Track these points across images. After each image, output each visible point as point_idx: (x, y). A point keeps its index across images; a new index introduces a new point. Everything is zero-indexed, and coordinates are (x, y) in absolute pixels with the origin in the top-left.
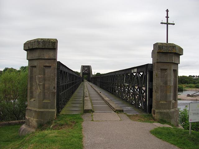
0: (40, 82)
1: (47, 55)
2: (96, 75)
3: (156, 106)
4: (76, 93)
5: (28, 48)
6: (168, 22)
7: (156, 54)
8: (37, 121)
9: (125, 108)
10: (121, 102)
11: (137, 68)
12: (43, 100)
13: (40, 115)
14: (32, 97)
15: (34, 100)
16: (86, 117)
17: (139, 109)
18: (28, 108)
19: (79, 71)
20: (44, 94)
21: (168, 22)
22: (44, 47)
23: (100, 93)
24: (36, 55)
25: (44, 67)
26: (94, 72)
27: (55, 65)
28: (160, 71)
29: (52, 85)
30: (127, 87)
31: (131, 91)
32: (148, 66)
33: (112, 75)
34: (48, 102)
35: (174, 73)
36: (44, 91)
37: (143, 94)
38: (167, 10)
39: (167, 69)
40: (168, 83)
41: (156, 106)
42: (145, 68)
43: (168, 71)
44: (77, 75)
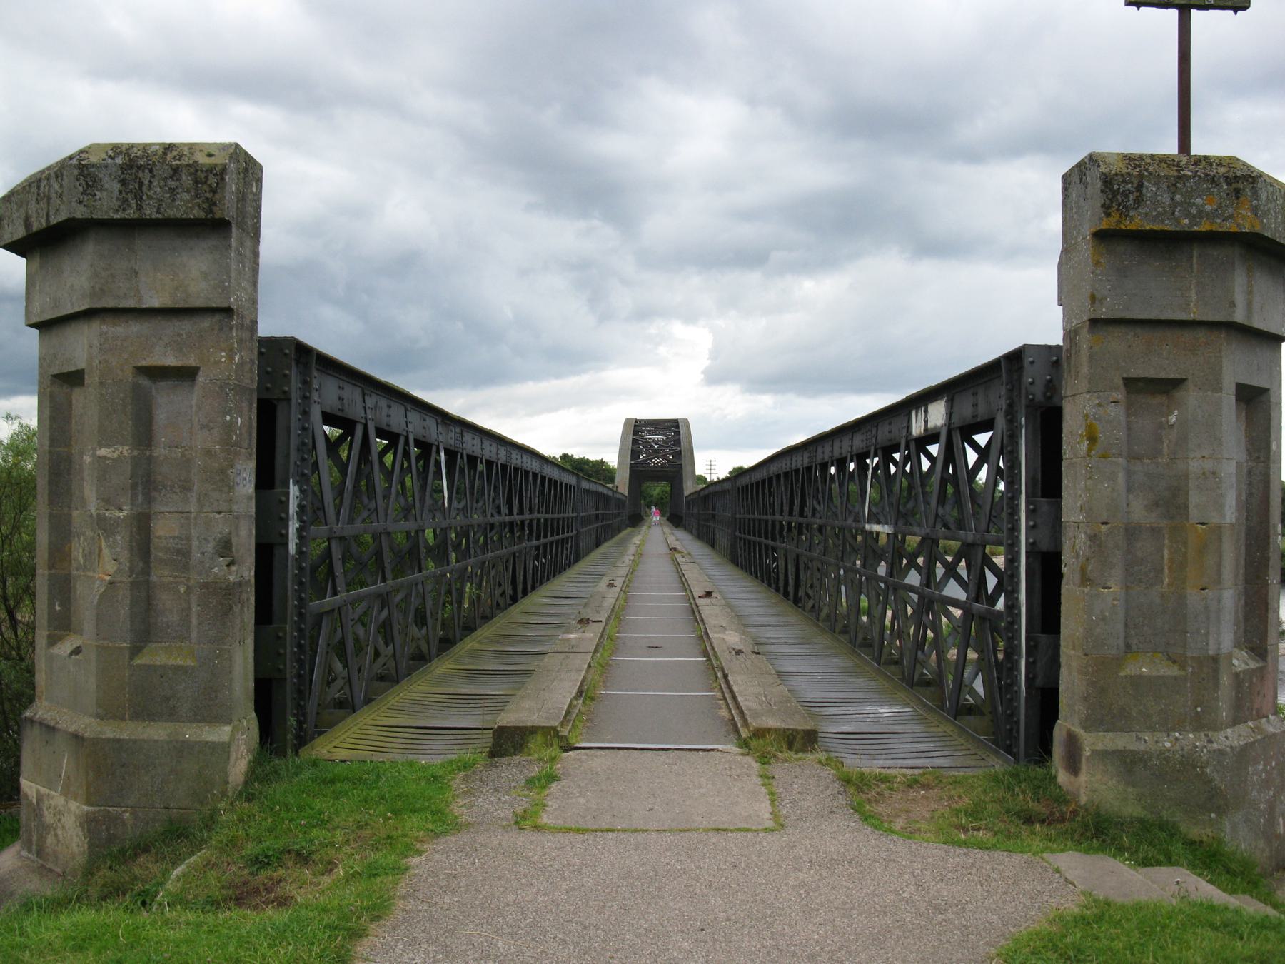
0: (107, 501)
1: (188, 273)
3: (1086, 699)
4: (539, 599)
5: (20, 233)
7: (1086, 246)
8: (89, 824)
9: (851, 710)
10: (838, 662)
11: (949, 390)
12: (135, 651)
13: (105, 767)
14: (63, 624)
15: (77, 651)
16: (492, 798)
17: (973, 720)
18: (41, 710)
19: (611, 458)
20: (149, 599)
22: (131, 213)
23: (709, 594)
24: (78, 278)
25: (144, 382)
26: (713, 462)
28: (1119, 396)
29: (215, 515)
30: (920, 560)
31: (954, 590)
32: (1021, 368)
33: (797, 471)
34: (178, 668)
35: (1250, 421)
36: (147, 571)
37: (993, 600)
39: (1177, 383)
40: (1195, 499)
41: (1086, 699)
42: (1003, 391)
43: (1191, 397)
44: (610, 493)
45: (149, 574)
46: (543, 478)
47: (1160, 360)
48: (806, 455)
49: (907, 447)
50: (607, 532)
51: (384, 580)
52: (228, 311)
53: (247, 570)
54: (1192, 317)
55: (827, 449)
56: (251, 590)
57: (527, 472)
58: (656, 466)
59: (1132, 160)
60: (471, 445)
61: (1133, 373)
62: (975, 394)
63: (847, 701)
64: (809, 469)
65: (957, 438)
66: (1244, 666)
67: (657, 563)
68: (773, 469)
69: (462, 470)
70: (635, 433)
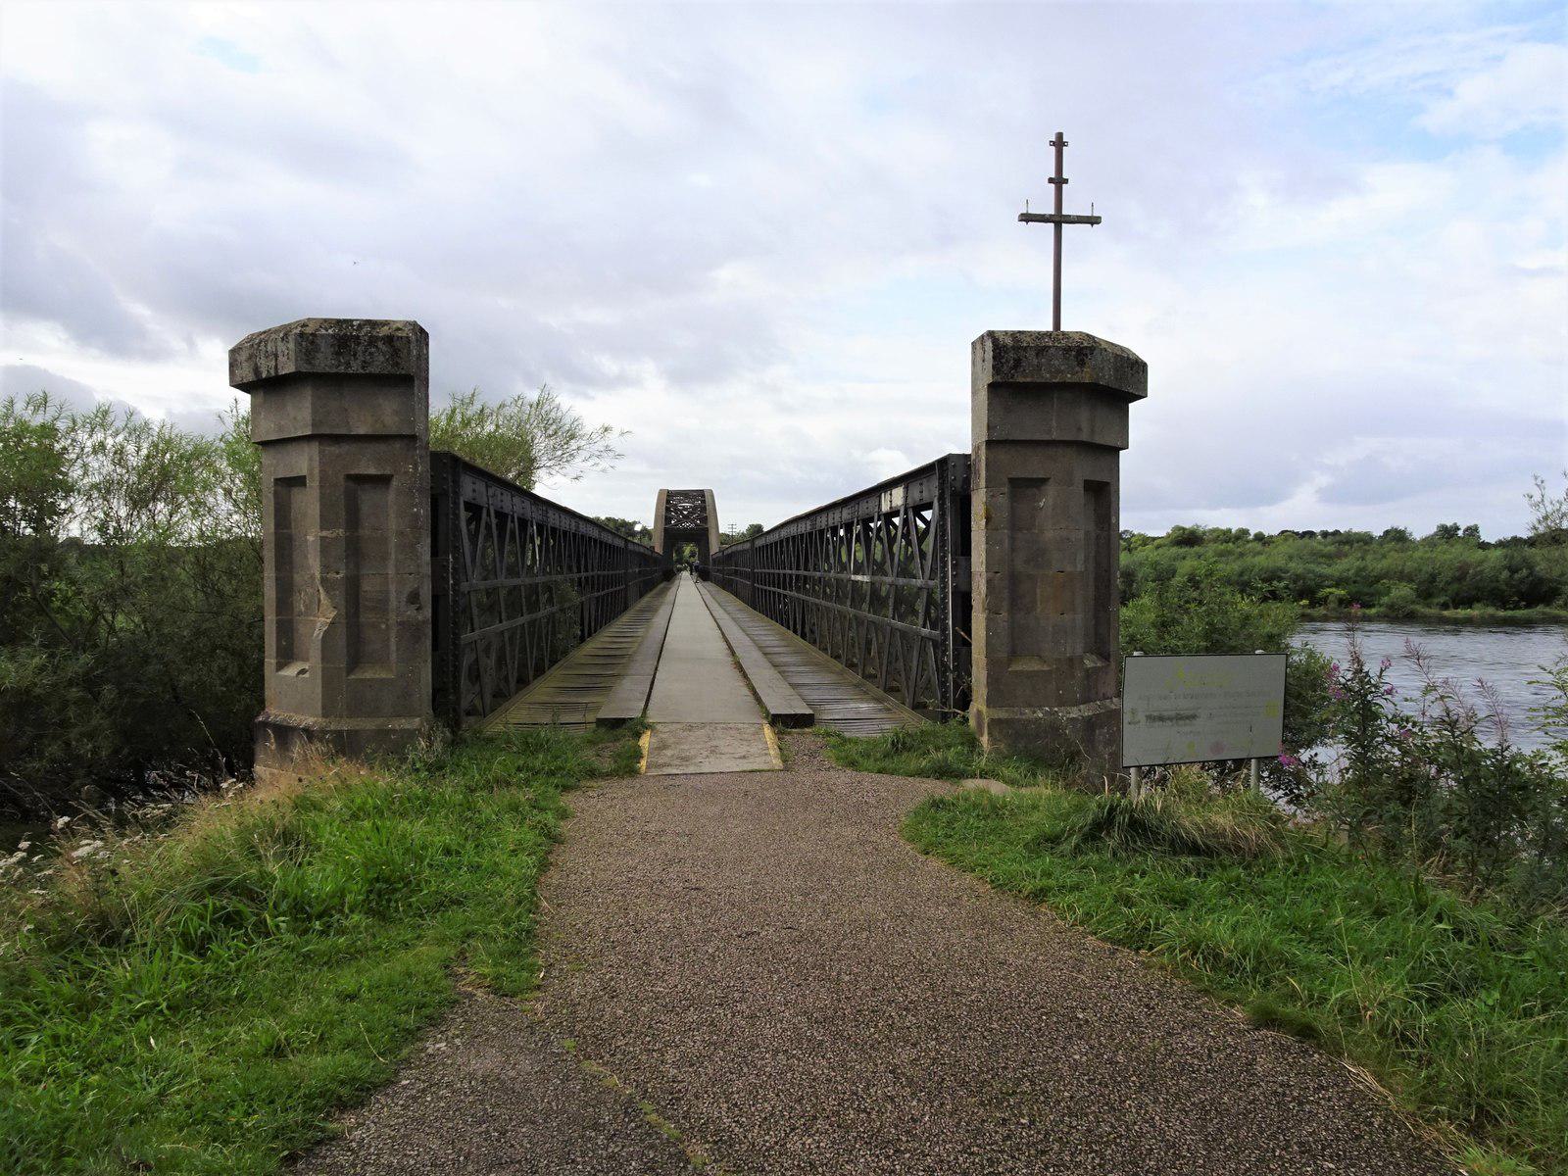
1: (381, 413)
2: (741, 539)
5: (251, 377)
6: (1065, 212)
9: (841, 706)
14: (286, 656)
15: (303, 671)
21: (1065, 212)
25: (351, 485)
26: (732, 519)
27: (415, 468)
29: (401, 574)
33: (802, 535)
36: (357, 614)
38: (1060, 136)
39: (1044, 481)
45: (358, 617)
46: (601, 542)
47: (1032, 466)
48: (809, 523)
49: (906, 513)
50: (647, 587)
51: (501, 622)
52: (413, 438)
53: (428, 612)
54: (1055, 436)
55: (824, 519)
56: (430, 626)
57: (590, 538)
58: (685, 529)
59: (1016, 336)
60: (553, 519)
61: (1014, 475)
62: (921, 484)
63: (838, 701)
64: (811, 534)
65: (911, 515)
66: (1092, 665)
67: (691, 611)
68: (784, 533)
69: (488, 526)
70: (668, 502)
